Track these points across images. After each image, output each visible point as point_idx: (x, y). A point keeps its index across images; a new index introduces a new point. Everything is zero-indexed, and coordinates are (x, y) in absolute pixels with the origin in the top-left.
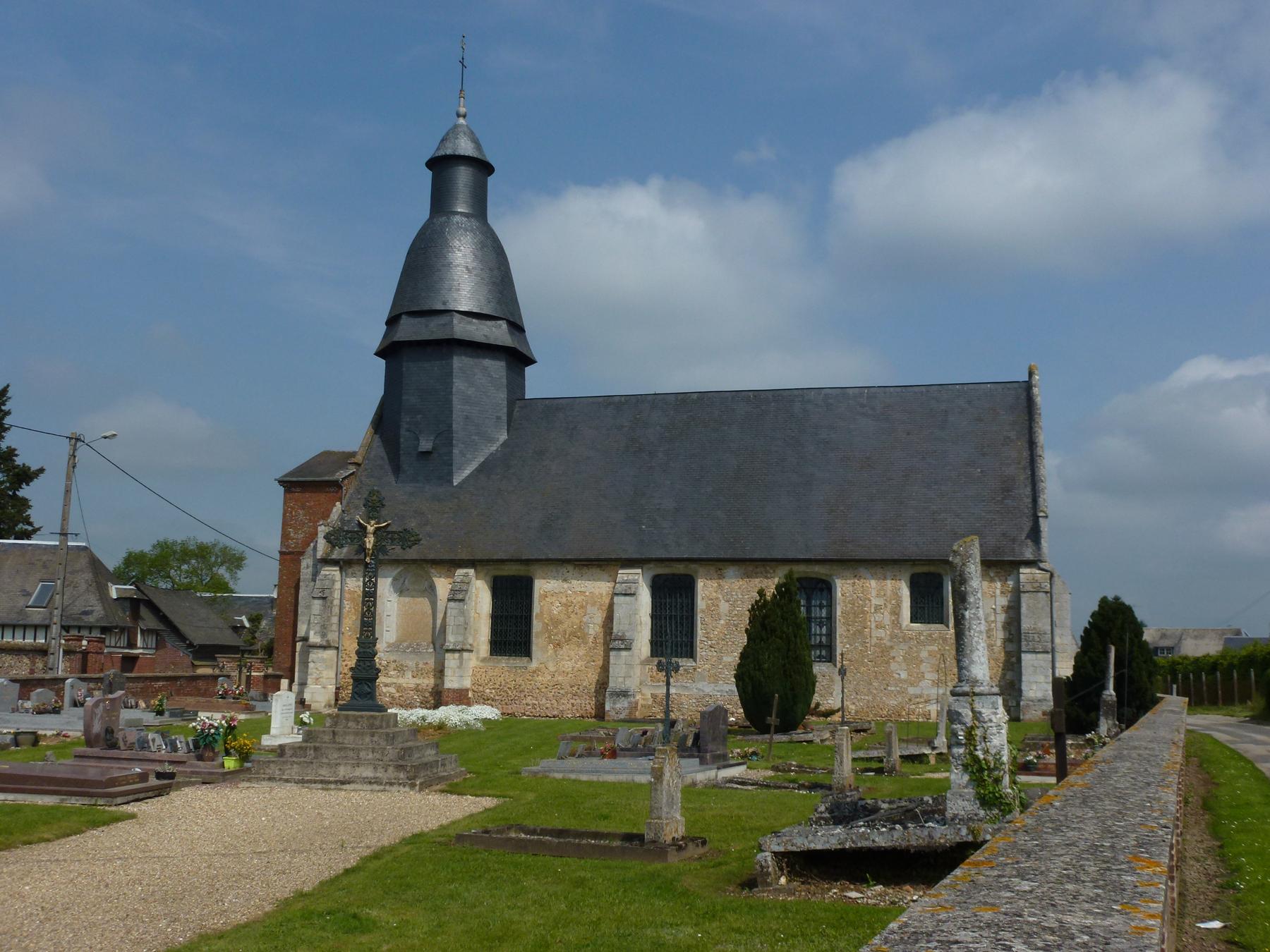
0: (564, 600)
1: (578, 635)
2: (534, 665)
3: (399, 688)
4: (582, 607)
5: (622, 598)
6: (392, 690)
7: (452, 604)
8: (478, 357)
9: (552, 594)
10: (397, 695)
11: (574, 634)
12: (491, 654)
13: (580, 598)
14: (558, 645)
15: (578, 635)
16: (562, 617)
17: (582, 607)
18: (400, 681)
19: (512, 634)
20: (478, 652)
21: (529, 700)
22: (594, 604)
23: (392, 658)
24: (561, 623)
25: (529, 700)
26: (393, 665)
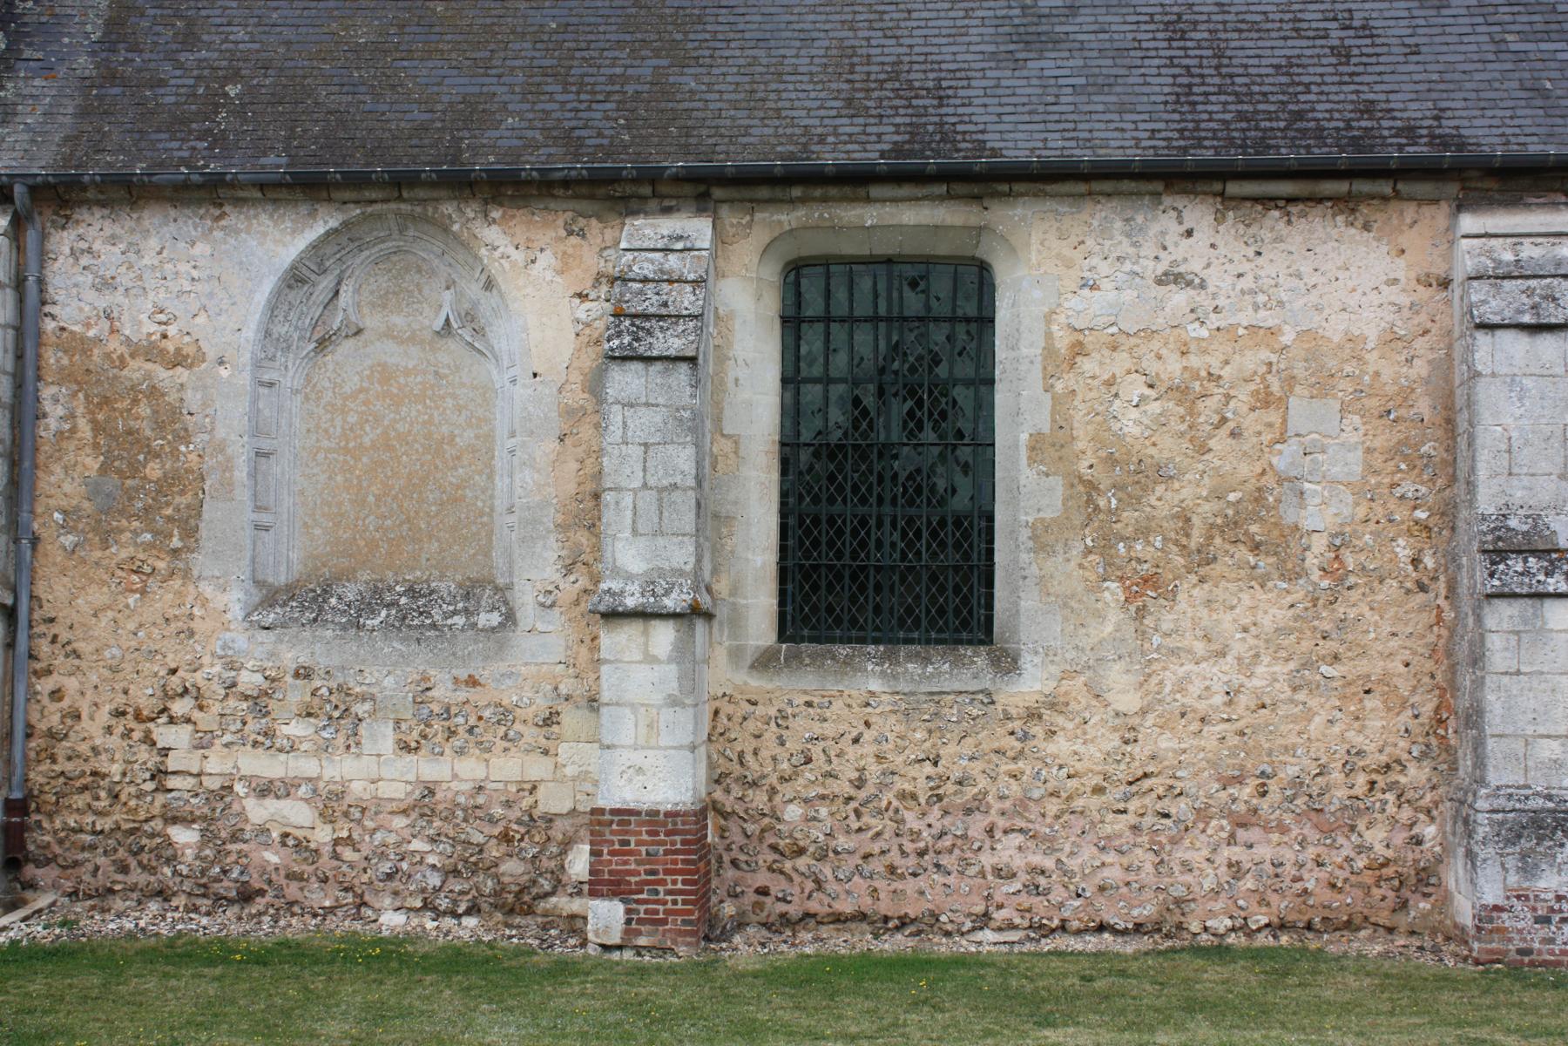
0: (1173, 367)
1: (1253, 531)
2: (1031, 683)
3: (332, 804)
4: (1265, 400)
5: (1515, 345)
6: (297, 813)
7: (627, 381)
8: (1440, 184)
9: (1096, 320)
10: (322, 836)
11: (1231, 527)
12: (782, 636)
13: (1252, 360)
14: (1146, 588)
15: (1253, 531)
16: (1168, 448)
17: (1265, 400)
18: (344, 769)
19: (886, 532)
20: (736, 622)
21: (1008, 851)
22: (1322, 387)
23: (291, 657)
24: (1163, 474)
25: (1008, 851)
26: (297, 694)
